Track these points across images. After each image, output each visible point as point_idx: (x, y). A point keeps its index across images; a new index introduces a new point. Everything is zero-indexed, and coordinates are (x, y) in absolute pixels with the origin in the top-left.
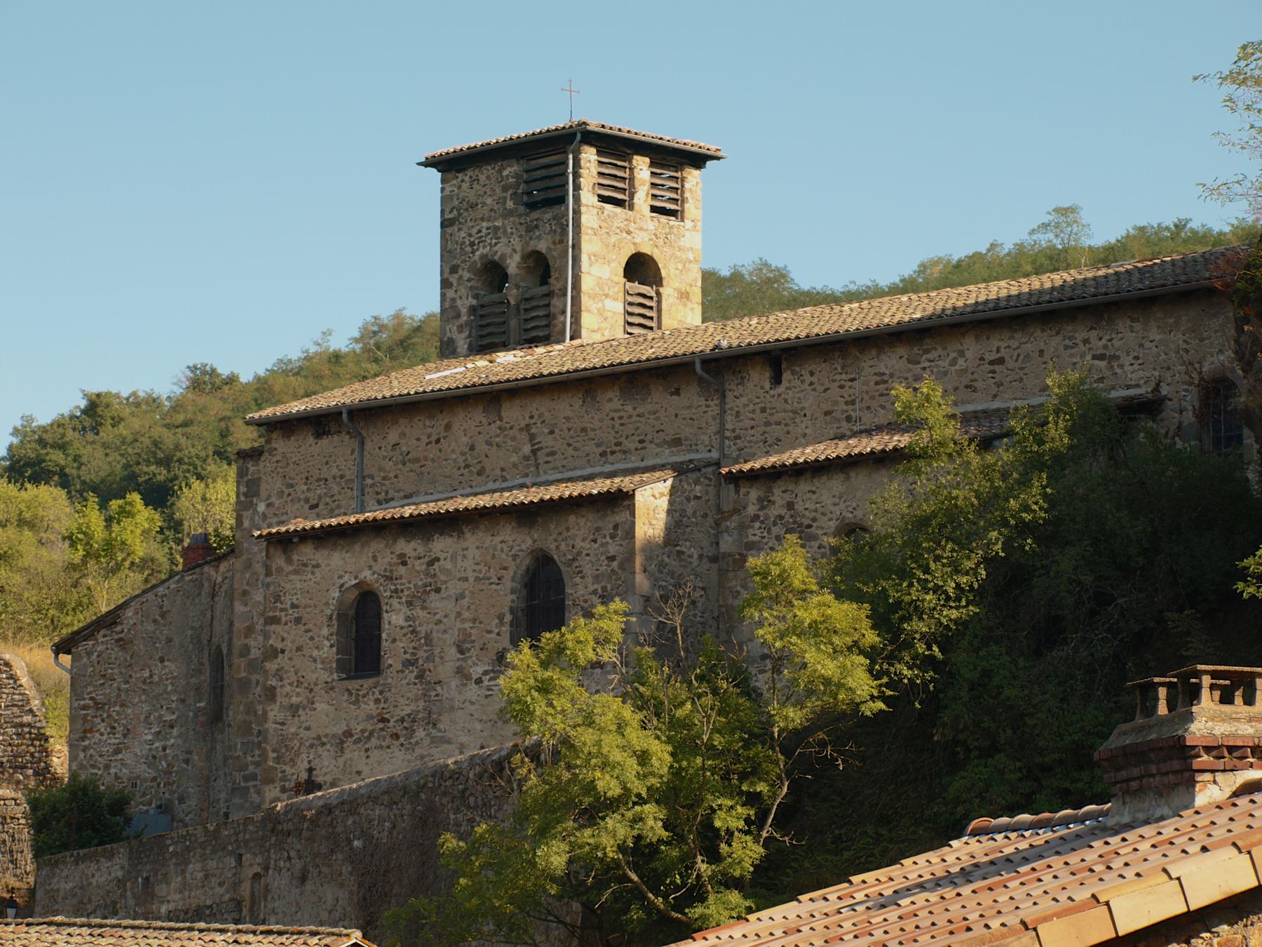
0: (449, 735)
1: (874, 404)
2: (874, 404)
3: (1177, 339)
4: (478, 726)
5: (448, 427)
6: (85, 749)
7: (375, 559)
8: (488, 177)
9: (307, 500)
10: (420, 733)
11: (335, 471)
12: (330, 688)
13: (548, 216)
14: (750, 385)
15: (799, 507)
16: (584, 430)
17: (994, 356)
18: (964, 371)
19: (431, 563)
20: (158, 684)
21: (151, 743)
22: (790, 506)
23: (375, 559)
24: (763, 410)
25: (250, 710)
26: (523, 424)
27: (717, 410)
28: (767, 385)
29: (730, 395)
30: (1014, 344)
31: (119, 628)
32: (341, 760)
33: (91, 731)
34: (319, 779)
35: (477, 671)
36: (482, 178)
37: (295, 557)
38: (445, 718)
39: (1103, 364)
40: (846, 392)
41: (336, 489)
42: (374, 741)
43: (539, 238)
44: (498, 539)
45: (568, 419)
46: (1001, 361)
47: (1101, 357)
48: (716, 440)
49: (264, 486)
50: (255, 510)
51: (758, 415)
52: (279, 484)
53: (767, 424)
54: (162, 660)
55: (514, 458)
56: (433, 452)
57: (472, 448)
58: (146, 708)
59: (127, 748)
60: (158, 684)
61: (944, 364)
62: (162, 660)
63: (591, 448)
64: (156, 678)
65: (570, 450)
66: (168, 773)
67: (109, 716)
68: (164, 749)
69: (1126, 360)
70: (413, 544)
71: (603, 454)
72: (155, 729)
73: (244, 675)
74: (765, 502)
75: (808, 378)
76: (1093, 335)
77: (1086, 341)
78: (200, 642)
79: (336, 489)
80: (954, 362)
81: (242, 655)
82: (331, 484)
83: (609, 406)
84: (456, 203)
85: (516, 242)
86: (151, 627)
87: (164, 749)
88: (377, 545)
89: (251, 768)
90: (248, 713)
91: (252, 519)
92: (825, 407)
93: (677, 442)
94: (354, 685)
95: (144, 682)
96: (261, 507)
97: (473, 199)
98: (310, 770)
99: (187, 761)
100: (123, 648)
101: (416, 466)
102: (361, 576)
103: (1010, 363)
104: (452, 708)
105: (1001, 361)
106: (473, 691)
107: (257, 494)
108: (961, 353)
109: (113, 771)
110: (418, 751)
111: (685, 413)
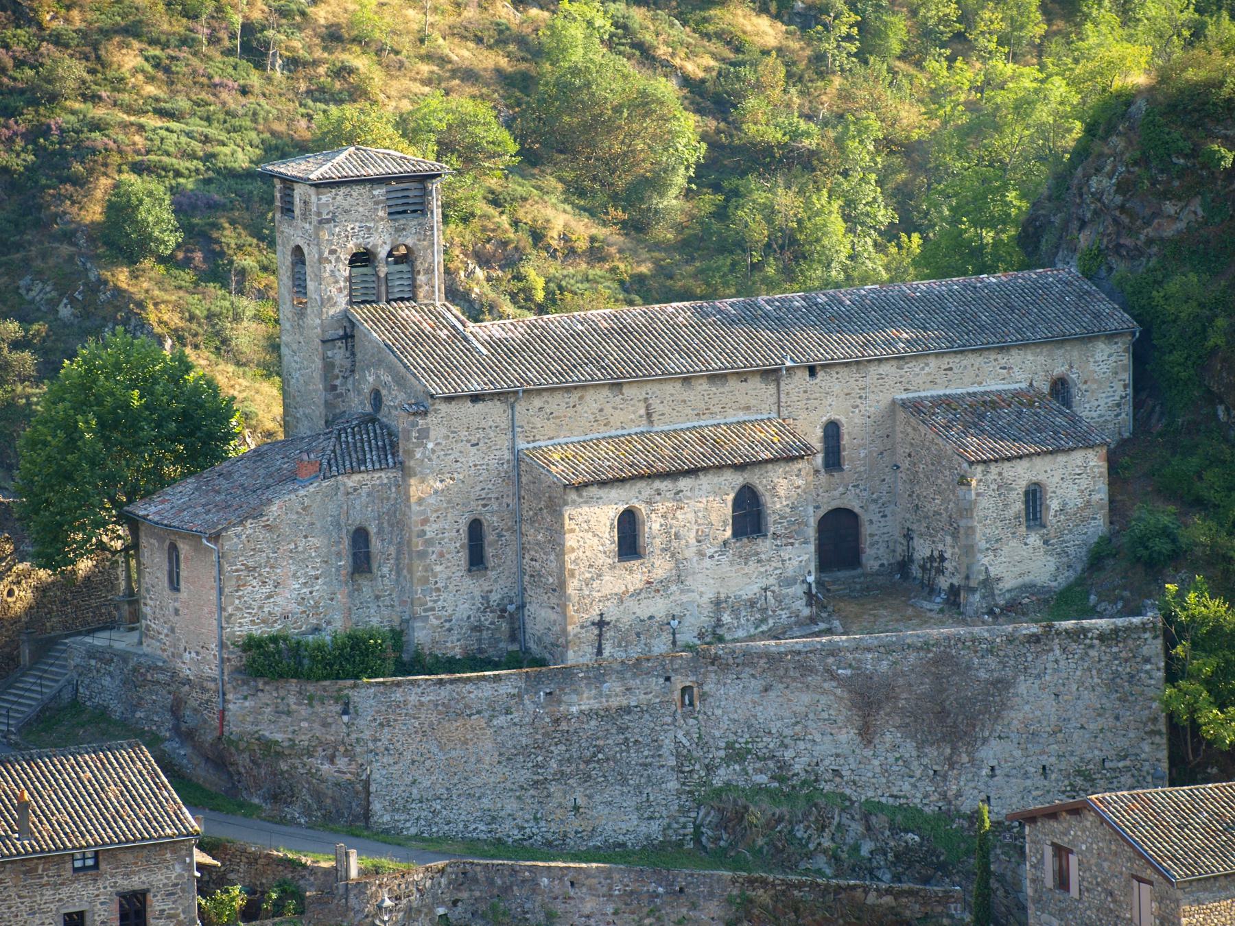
0: (693, 588)
3: (1041, 359)
4: (712, 581)
5: (581, 398)
6: (240, 598)
7: (640, 492)
8: (360, 194)
9: (468, 441)
10: (674, 588)
12: (612, 567)
13: (415, 223)
14: (796, 378)
15: (1005, 474)
16: (684, 401)
17: (946, 366)
18: (929, 374)
20: (303, 552)
21: (299, 590)
22: (1000, 474)
24: (805, 392)
25: (428, 568)
26: (641, 397)
28: (808, 378)
29: (782, 384)
32: (622, 608)
34: (608, 619)
36: (355, 194)
37: (585, 494)
38: (690, 578)
39: (1004, 371)
40: (860, 383)
41: (492, 434)
42: (643, 595)
45: (672, 395)
46: (951, 369)
47: (1004, 368)
48: (775, 408)
49: (432, 434)
50: (425, 447)
51: (801, 394)
52: (444, 431)
53: (808, 399)
54: (306, 537)
55: (633, 416)
56: (570, 412)
58: (293, 568)
59: (277, 595)
61: (917, 370)
62: (306, 537)
64: (300, 549)
65: (675, 413)
66: (316, 606)
69: (1016, 369)
70: (665, 483)
71: (698, 415)
72: (302, 580)
73: (421, 548)
75: (835, 376)
76: (999, 357)
77: (996, 360)
78: (339, 524)
79: (492, 434)
80: (923, 369)
81: (419, 536)
82: (488, 431)
84: (331, 208)
86: (294, 517)
88: (641, 485)
89: (430, 604)
90: (426, 571)
91: (423, 453)
92: (846, 391)
93: (748, 408)
94: (628, 564)
95: (291, 551)
96: (430, 445)
97: (348, 207)
98: (601, 615)
99: (332, 599)
101: (558, 421)
103: (955, 370)
104: (694, 573)
105: (951, 369)
106: (707, 563)
107: (427, 437)
108: (927, 365)
109: (266, 610)
110: (672, 598)
111: (754, 393)
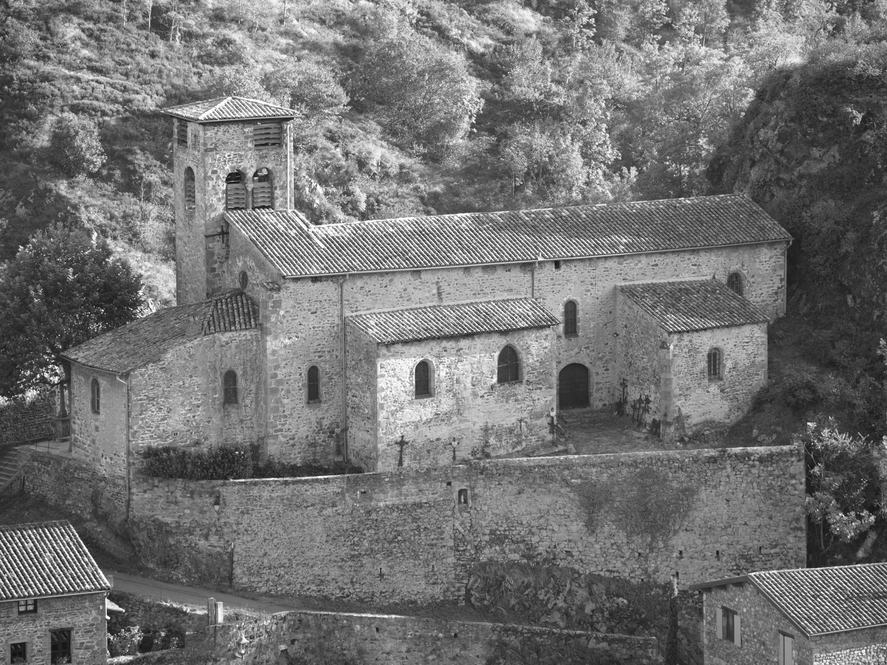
1: (603, 279)
2: (603, 279)
3: (721, 259)
4: (482, 414)
6: (142, 419)
7: (432, 349)
8: (235, 131)
9: (309, 310)
10: (455, 418)
11: (326, 297)
14: (546, 269)
15: (694, 341)
16: (465, 284)
17: (654, 263)
18: (641, 268)
19: (458, 350)
20: (188, 388)
21: (185, 414)
22: (691, 341)
23: (432, 349)
24: (552, 279)
27: (530, 278)
29: (536, 273)
30: (661, 259)
31: (162, 363)
32: (417, 432)
33: (146, 410)
34: (407, 440)
35: (481, 393)
36: (231, 131)
40: (591, 274)
41: (326, 306)
43: (268, 162)
44: (491, 341)
45: (456, 280)
46: (657, 265)
47: (695, 265)
48: (530, 290)
49: (283, 304)
50: (278, 314)
51: (549, 281)
52: (292, 302)
53: (554, 285)
54: (191, 376)
55: (428, 295)
56: (383, 291)
57: (405, 290)
58: (181, 399)
59: (170, 418)
60: (188, 388)
61: (632, 265)
62: (191, 376)
63: (468, 291)
64: (187, 385)
67: (158, 403)
68: (194, 417)
69: (704, 266)
70: (450, 343)
71: (475, 294)
72: (187, 408)
73: (273, 386)
74: (680, 340)
75: (574, 268)
76: (692, 257)
77: (689, 259)
78: (215, 368)
79: (326, 306)
80: (636, 265)
82: (324, 303)
83: (476, 275)
84: (214, 141)
85: (253, 162)
86: (183, 362)
87: (194, 417)
88: (433, 344)
89: (279, 427)
91: (277, 318)
92: (582, 279)
93: (511, 290)
95: (180, 387)
96: (282, 313)
97: (226, 140)
98: (402, 437)
99: (209, 422)
100: (165, 372)
101: (374, 297)
102: (425, 357)
103: (660, 266)
105: (657, 265)
106: (479, 401)
108: (640, 262)
109: (161, 428)
110: (453, 426)
111: (515, 279)
